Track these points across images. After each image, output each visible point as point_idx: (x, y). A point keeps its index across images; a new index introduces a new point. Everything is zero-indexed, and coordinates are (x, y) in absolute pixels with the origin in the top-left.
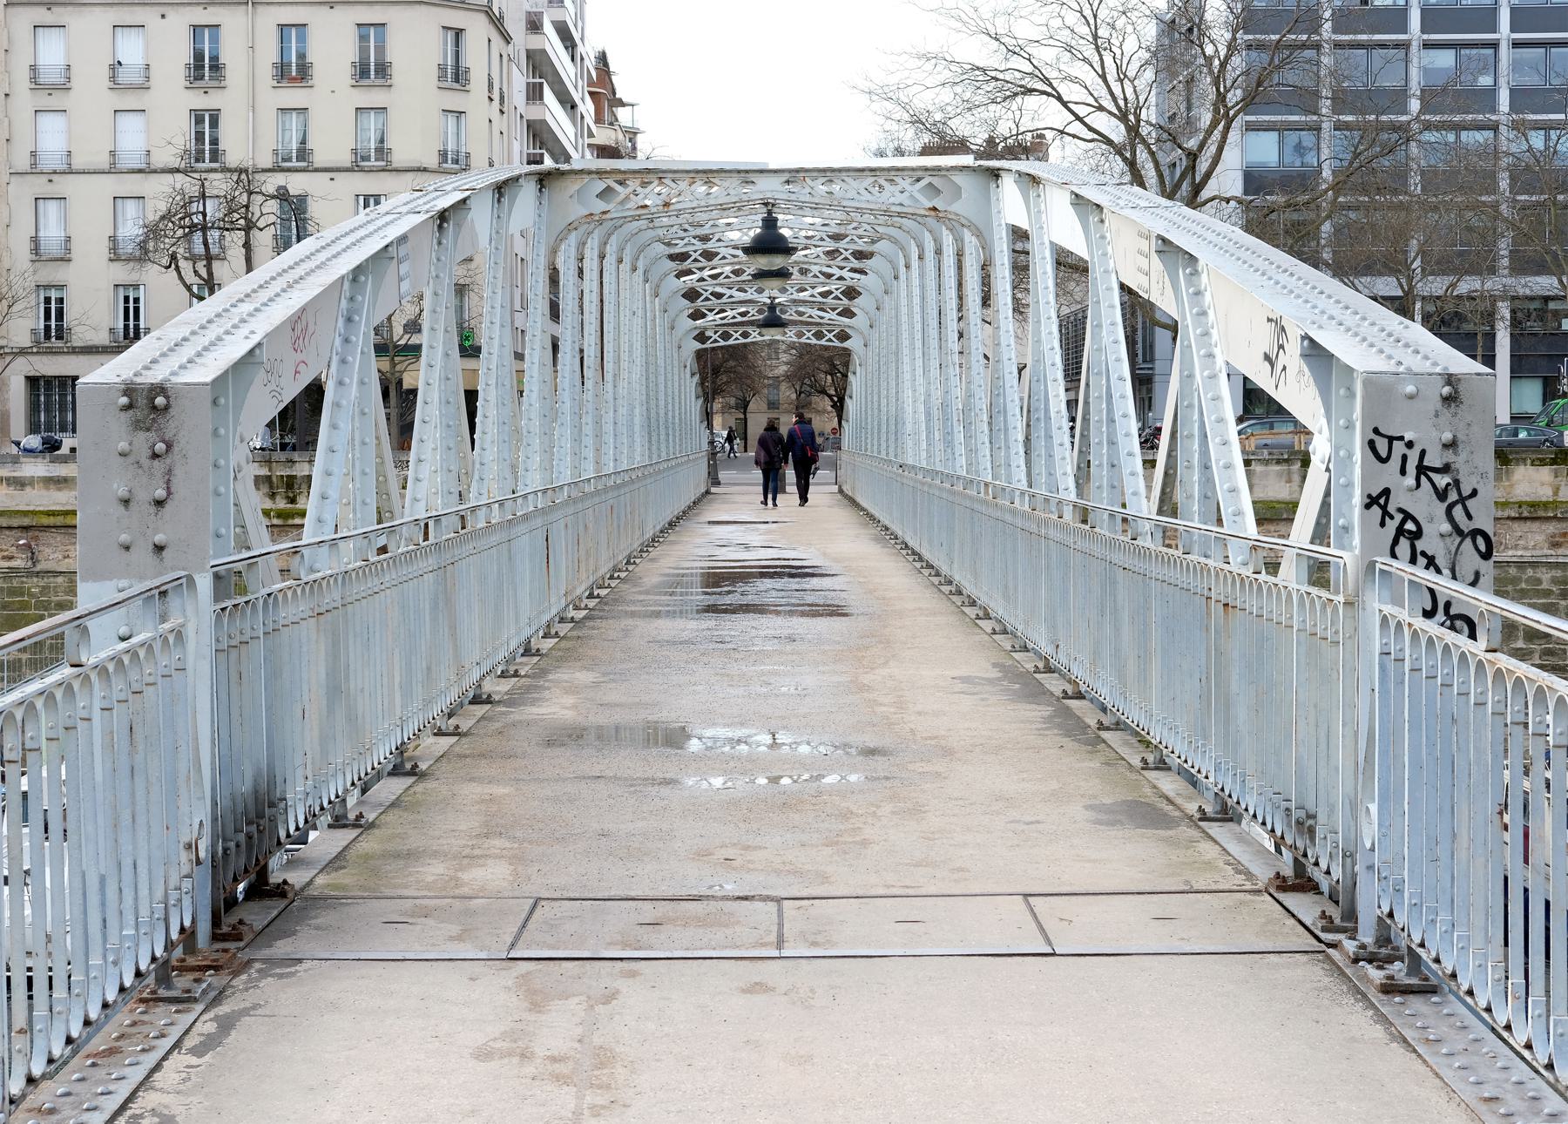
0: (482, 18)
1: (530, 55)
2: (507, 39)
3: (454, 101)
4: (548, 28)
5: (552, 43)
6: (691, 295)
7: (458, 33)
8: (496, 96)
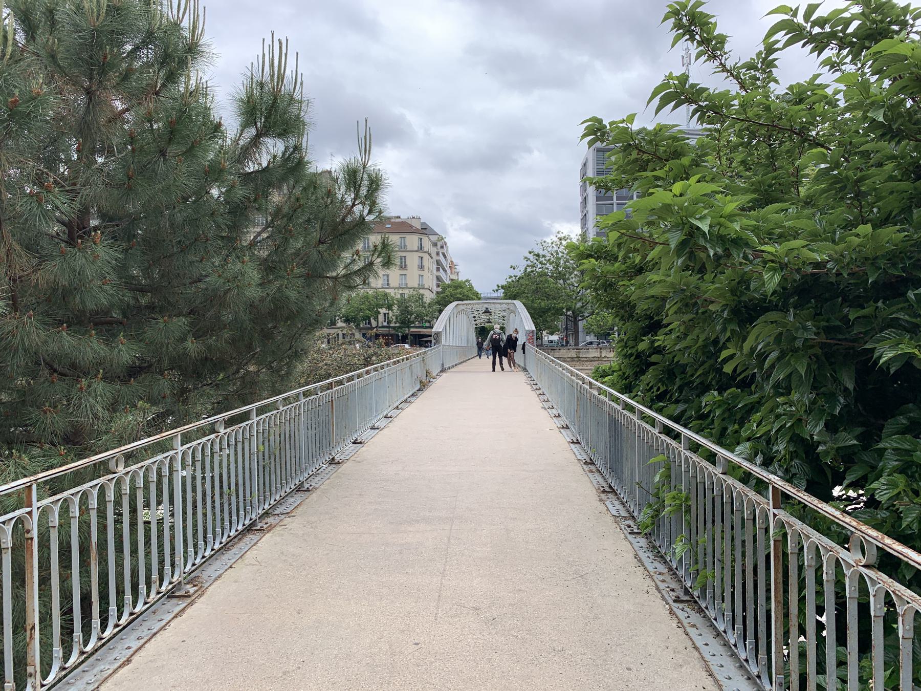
3: (421, 273)
5: (441, 258)
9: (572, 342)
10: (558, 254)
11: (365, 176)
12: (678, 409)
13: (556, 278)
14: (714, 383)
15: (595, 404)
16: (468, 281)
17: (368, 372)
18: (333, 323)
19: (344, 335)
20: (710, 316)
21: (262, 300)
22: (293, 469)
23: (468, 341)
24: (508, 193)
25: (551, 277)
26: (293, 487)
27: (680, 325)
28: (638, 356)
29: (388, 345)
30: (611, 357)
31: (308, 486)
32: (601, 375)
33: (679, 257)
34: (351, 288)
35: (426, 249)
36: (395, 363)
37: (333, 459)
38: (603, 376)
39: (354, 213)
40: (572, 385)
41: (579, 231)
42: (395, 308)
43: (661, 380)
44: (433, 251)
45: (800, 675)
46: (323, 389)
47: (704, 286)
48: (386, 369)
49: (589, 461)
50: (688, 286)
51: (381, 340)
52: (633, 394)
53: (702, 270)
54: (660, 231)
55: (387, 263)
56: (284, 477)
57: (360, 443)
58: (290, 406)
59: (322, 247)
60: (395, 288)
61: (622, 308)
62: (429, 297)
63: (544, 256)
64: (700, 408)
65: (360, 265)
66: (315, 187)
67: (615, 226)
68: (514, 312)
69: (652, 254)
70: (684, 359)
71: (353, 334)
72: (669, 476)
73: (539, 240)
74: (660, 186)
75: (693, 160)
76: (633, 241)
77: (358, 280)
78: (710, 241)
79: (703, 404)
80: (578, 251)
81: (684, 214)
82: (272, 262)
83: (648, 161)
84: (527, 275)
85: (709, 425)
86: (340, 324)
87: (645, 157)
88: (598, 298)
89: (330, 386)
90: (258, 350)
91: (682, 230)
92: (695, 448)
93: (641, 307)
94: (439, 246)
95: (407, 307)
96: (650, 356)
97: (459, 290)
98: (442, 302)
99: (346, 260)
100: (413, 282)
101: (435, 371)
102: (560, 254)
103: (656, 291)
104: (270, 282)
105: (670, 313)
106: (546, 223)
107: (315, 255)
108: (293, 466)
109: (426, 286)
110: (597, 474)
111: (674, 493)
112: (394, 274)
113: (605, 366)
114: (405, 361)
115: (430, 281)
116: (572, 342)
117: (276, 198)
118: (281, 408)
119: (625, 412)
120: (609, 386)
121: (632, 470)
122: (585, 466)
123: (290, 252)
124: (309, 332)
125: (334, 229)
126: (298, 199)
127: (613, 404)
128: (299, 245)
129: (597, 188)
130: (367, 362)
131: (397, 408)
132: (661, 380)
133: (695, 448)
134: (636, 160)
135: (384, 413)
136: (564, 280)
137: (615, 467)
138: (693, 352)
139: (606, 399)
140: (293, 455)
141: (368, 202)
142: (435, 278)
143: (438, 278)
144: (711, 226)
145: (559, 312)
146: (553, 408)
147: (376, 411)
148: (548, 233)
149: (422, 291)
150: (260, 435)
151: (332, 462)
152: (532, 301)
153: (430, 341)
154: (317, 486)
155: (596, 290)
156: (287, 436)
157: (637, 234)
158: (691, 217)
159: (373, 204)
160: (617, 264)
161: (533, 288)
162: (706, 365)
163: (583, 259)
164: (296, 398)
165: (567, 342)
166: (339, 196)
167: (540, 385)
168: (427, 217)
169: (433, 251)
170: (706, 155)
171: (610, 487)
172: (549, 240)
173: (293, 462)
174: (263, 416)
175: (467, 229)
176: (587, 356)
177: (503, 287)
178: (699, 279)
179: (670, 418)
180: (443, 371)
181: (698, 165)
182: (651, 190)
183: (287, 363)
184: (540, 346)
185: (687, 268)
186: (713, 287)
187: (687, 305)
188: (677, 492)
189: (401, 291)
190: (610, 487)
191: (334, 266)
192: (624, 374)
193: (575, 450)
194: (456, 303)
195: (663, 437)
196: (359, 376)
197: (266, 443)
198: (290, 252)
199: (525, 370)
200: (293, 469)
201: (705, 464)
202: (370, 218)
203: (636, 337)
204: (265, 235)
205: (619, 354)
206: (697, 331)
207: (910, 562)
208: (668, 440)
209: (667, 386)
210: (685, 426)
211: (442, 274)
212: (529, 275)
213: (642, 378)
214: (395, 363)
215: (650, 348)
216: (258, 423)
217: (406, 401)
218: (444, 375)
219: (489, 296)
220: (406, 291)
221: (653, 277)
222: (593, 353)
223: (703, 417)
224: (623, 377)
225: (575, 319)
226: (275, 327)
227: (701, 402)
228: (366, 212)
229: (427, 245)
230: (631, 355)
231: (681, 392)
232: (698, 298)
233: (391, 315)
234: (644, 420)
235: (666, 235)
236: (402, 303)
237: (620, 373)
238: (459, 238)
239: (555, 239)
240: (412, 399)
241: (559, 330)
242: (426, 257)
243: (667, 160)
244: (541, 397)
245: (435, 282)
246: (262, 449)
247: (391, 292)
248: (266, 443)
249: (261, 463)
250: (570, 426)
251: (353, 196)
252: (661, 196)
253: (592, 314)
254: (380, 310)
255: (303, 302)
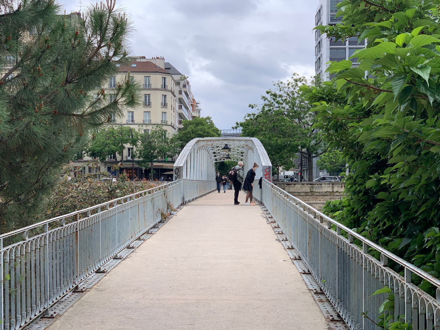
0: (170, 93)
1: (179, 99)
2: (175, 96)
3: (164, 110)
4: (183, 93)
5: (184, 96)
6: (214, 153)
7: (165, 96)
8: (173, 109)
9: (306, 177)
10: (293, 94)
11: (111, 20)
12: (402, 243)
13: (292, 117)
14: (435, 219)
15: (326, 238)
16: (208, 118)
17: (111, 205)
18: (80, 157)
19: (90, 168)
20: (432, 157)
21: (11, 136)
22: (38, 297)
23: (208, 176)
24: (247, 35)
25: (287, 116)
26: (38, 314)
27: (404, 165)
28: (367, 192)
29: (131, 178)
30: (340, 192)
31: (52, 313)
32: (331, 210)
33: (401, 103)
34: (96, 125)
35: (169, 88)
36: (137, 196)
37: (77, 287)
38: (334, 211)
39: (100, 54)
40: (305, 219)
41: (314, 74)
42: (139, 143)
43: (386, 216)
46: (68, 220)
47: (426, 129)
48: (129, 202)
49: (319, 291)
50: (411, 130)
51: (125, 174)
52: (361, 229)
53: (424, 115)
54: (384, 79)
55: (131, 102)
56: (29, 305)
57: (103, 272)
58: (36, 237)
59: (69, 87)
60: (139, 125)
61: (352, 147)
62: (171, 133)
63: (280, 96)
64: (423, 243)
65: (105, 103)
66: (63, 30)
67: (342, 74)
68: (252, 148)
69: (378, 99)
70: (408, 197)
71: (98, 168)
72: (393, 307)
73: (276, 81)
74: (386, 36)
75: (417, 12)
76: (359, 88)
77: (103, 118)
78: (430, 89)
79: (426, 239)
80: (310, 94)
81: (407, 64)
82: (21, 99)
83: (376, 12)
84: (264, 114)
85: (431, 259)
86: (87, 158)
87: (372, 8)
88: (329, 138)
89: (75, 218)
90: (6, 183)
91: (405, 78)
92: (417, 281)
93: (368, 148)
94: (181, 85)
95: (150, 142)
96: (376, 193)
97: (200, 127)
98: (184, 138)
99: (94, 97)
100: (156, 118)
101: (175, 204)
102: (296, 95)
103: (382, 133)
104: (18, 119)
105: (395, 154)
106: (282, 65)
107: (62, 93)
108: (38, 294)
109: (169, 123)
110: (326, 304)
111: (397, 323)
112: (139, 113)
113: (335, 201)
114: (147, 195)
115: (172, 118)
116: (306, 177)
117: (26, 38)
118: (27, 239)
119: (353, 245)
120: (339, 221)
121: (359, 301)
122: (315, 296)
123: (38, 90)
124: (55, 167)
125: (81, 70)
126: (46, 41)
127: (342, 237)
128: (47, 84)
129: (328, 36)
130: (111, 195)
131: (139, 239)
132: (386, 216)
133: (417, 281)
134: (364, 11)
135: (127, 244)
136: (300, 119)
137: (343, 297)
138: (416, 190)
139: (336, 233)
140: (38, 283)
141: (113, 45)
142: (177, 115)
143: (181, 116)
144: (431, 75)
145: (294, 149)
146: (286, 240)
147: (119, 242)
148: (284, 74)
149: (164, 128)
150: (7, 265)
151: (76, 290)
152: (270, 138)
153: (172, 176)
154: (61, 313)
155: (327, 130)
156: (33, 265)
157: (362, 81)
158: (412, 66)
159: (118, 46)
160: (346, 107)
161: (271, 125)
162: (429, 203)
163: (315, 101)
164: (42, 229)
165: (302, 178)
166: (86, 39)
167: (275, 218)
168: (171, 58)
169: (176, 89)
170: (429, 7)
171: (339, 316)
172: (285, 81)
173: (38, 290)
174: (10, 247)
175: (208, 69)
176: (321, 190)
177: (242, 125)
178: (422, 123)
179: (395, 252)
180: (184, 204)
181: (421, 17)
182: (377, 40)
183: (35, 195)
184: (276, 181)
185: (411, 113)
186: (434, 131)
187: (410, 147)
188: (399, 322)
189: (144, 127)
190: (339, 316)
191: (81, 104)
192: (353, 209)
193: (306, 281)
194: (197, 139)
195: (388, 270)
196: (103, 208)
197: (13, 273)
198: (38, 90)
199: (261, 203)
200: (38, 297)
201: (426, 296)
202: (116, 59)
203: (364, 174)
204: (15, 74)
205: (348, 190)
206: (419, 171)
208: (392, 273)
209: (392, 221)
210: (408, 260)
211: (184, 111)
212: (266, 113)
213: (369, 213)
214: (137, 196)
215: (376, 186)
216: (5, 253)
217: (147, 232)
218: (185, 208)
219: (229, 132)
220: (150, 128)
221: (378, 120)
222: (326, 188)
223: (425, 251)
224: (352, 212)
225: (310, 156)
226: (22, 162)
227: (424, 237)
228: (111, 54)
229: (170, 84)
230: (360, 191)
231: (405, 228)
232: (421, 141)
233: (135, 149)
234: (371, 254)
235: (390, 83)
236: (146, 138)
237: (349, 208)
238: (200, 77)
239: (292, 81)
240: (154, 230)
241: (294, 166)
242: (169, 95)
243: (392, 12)
244: (276, 230)
245: (177, 119)
246: (8, 278)
247: (136, 128)
248: (13, 273)
249: (7, 291)
250: (302, 257)
251: (99, 39)
252: (386, 47)
253: (325, 151)
254: (125, 145)
255: (50, 138)
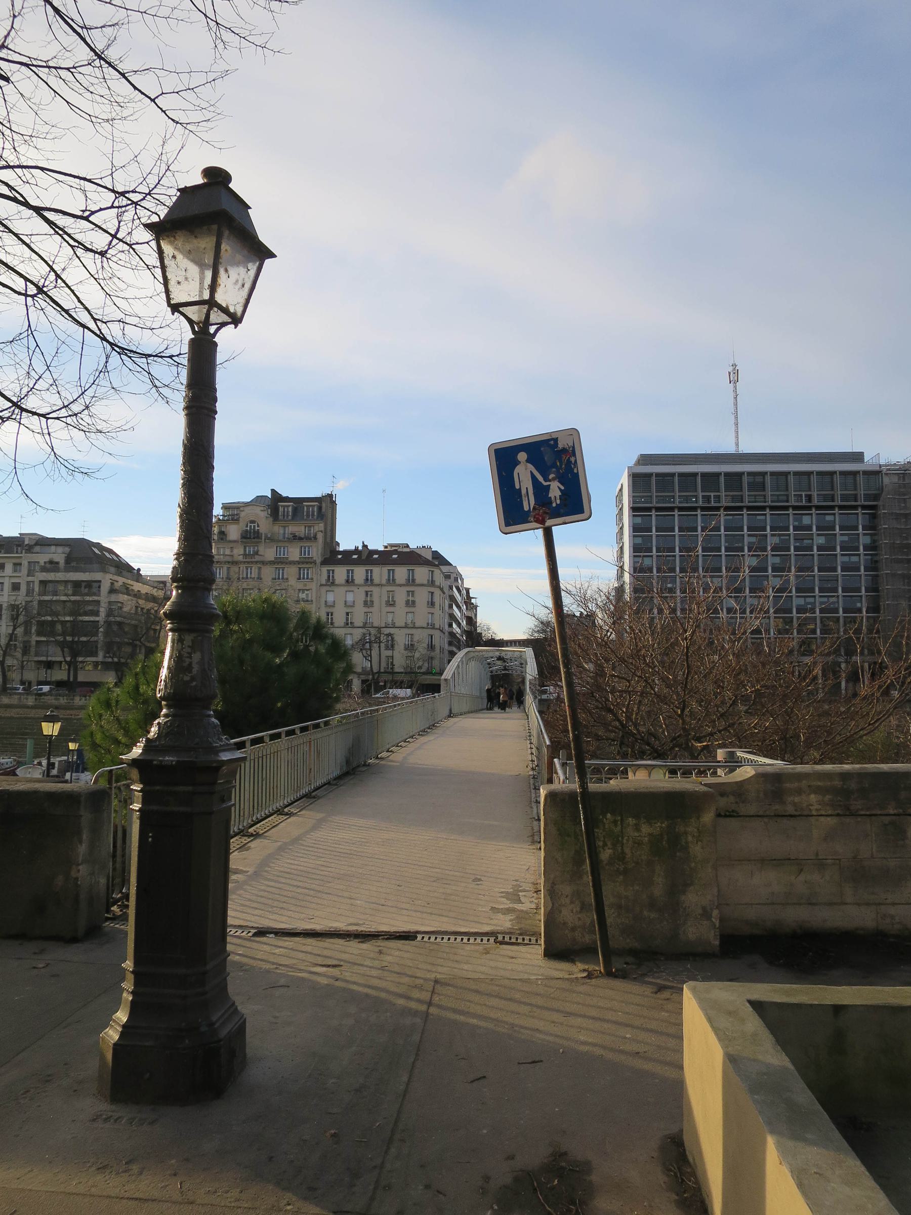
1: (450, 596)
3: (432, 610)
7: (432, 593)
35: (437, 583)
44: (445, 584)
45: (95, 683)
142: (447, 616)
207: (355, 987)
242: (437, 592)
